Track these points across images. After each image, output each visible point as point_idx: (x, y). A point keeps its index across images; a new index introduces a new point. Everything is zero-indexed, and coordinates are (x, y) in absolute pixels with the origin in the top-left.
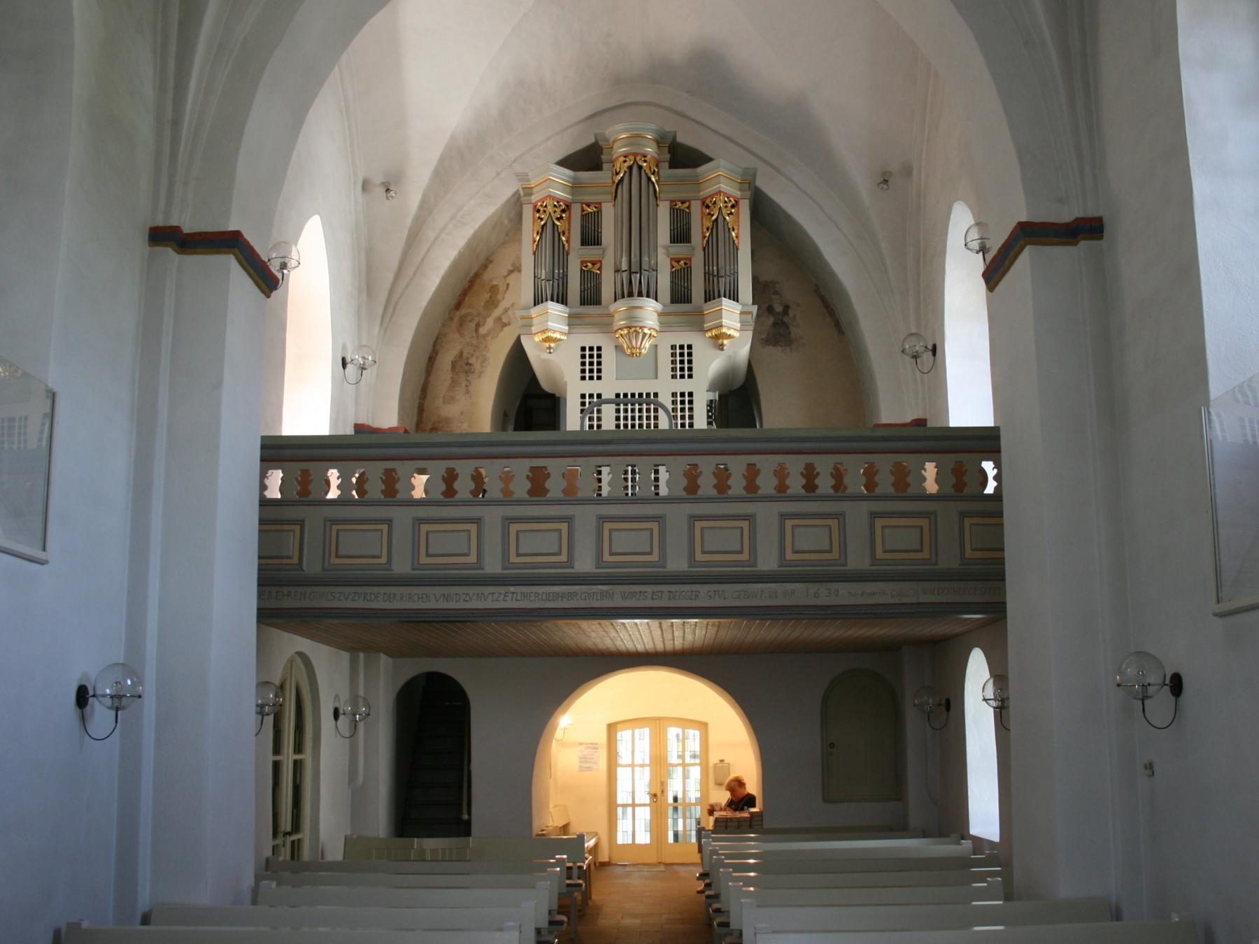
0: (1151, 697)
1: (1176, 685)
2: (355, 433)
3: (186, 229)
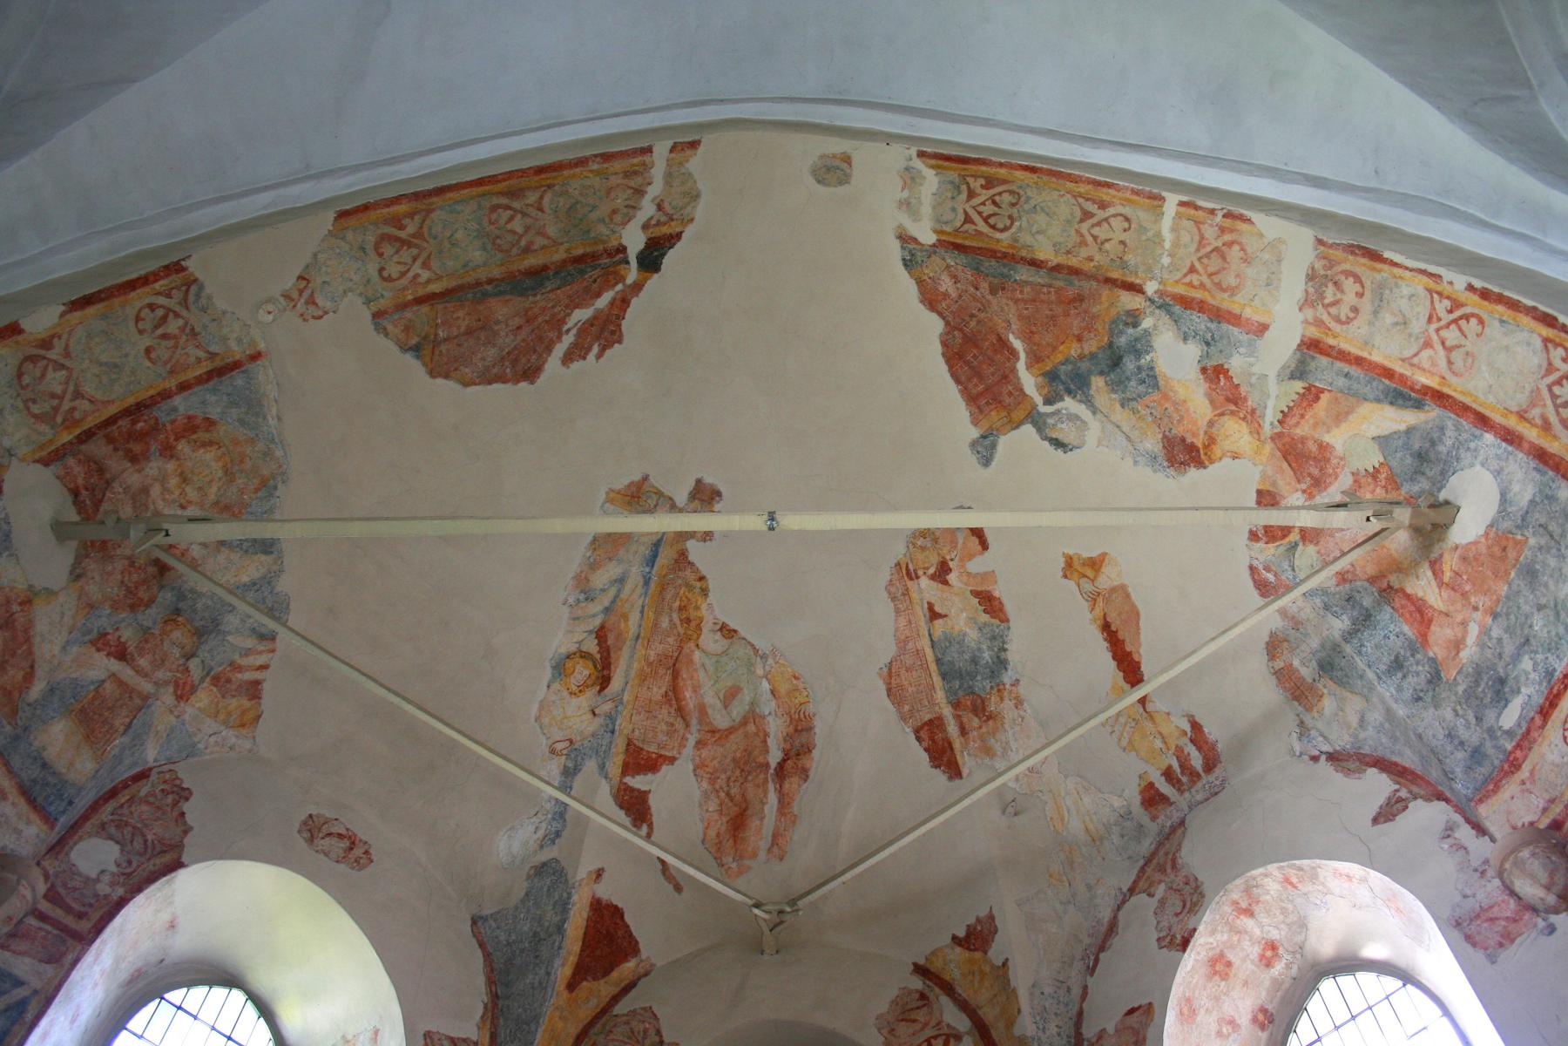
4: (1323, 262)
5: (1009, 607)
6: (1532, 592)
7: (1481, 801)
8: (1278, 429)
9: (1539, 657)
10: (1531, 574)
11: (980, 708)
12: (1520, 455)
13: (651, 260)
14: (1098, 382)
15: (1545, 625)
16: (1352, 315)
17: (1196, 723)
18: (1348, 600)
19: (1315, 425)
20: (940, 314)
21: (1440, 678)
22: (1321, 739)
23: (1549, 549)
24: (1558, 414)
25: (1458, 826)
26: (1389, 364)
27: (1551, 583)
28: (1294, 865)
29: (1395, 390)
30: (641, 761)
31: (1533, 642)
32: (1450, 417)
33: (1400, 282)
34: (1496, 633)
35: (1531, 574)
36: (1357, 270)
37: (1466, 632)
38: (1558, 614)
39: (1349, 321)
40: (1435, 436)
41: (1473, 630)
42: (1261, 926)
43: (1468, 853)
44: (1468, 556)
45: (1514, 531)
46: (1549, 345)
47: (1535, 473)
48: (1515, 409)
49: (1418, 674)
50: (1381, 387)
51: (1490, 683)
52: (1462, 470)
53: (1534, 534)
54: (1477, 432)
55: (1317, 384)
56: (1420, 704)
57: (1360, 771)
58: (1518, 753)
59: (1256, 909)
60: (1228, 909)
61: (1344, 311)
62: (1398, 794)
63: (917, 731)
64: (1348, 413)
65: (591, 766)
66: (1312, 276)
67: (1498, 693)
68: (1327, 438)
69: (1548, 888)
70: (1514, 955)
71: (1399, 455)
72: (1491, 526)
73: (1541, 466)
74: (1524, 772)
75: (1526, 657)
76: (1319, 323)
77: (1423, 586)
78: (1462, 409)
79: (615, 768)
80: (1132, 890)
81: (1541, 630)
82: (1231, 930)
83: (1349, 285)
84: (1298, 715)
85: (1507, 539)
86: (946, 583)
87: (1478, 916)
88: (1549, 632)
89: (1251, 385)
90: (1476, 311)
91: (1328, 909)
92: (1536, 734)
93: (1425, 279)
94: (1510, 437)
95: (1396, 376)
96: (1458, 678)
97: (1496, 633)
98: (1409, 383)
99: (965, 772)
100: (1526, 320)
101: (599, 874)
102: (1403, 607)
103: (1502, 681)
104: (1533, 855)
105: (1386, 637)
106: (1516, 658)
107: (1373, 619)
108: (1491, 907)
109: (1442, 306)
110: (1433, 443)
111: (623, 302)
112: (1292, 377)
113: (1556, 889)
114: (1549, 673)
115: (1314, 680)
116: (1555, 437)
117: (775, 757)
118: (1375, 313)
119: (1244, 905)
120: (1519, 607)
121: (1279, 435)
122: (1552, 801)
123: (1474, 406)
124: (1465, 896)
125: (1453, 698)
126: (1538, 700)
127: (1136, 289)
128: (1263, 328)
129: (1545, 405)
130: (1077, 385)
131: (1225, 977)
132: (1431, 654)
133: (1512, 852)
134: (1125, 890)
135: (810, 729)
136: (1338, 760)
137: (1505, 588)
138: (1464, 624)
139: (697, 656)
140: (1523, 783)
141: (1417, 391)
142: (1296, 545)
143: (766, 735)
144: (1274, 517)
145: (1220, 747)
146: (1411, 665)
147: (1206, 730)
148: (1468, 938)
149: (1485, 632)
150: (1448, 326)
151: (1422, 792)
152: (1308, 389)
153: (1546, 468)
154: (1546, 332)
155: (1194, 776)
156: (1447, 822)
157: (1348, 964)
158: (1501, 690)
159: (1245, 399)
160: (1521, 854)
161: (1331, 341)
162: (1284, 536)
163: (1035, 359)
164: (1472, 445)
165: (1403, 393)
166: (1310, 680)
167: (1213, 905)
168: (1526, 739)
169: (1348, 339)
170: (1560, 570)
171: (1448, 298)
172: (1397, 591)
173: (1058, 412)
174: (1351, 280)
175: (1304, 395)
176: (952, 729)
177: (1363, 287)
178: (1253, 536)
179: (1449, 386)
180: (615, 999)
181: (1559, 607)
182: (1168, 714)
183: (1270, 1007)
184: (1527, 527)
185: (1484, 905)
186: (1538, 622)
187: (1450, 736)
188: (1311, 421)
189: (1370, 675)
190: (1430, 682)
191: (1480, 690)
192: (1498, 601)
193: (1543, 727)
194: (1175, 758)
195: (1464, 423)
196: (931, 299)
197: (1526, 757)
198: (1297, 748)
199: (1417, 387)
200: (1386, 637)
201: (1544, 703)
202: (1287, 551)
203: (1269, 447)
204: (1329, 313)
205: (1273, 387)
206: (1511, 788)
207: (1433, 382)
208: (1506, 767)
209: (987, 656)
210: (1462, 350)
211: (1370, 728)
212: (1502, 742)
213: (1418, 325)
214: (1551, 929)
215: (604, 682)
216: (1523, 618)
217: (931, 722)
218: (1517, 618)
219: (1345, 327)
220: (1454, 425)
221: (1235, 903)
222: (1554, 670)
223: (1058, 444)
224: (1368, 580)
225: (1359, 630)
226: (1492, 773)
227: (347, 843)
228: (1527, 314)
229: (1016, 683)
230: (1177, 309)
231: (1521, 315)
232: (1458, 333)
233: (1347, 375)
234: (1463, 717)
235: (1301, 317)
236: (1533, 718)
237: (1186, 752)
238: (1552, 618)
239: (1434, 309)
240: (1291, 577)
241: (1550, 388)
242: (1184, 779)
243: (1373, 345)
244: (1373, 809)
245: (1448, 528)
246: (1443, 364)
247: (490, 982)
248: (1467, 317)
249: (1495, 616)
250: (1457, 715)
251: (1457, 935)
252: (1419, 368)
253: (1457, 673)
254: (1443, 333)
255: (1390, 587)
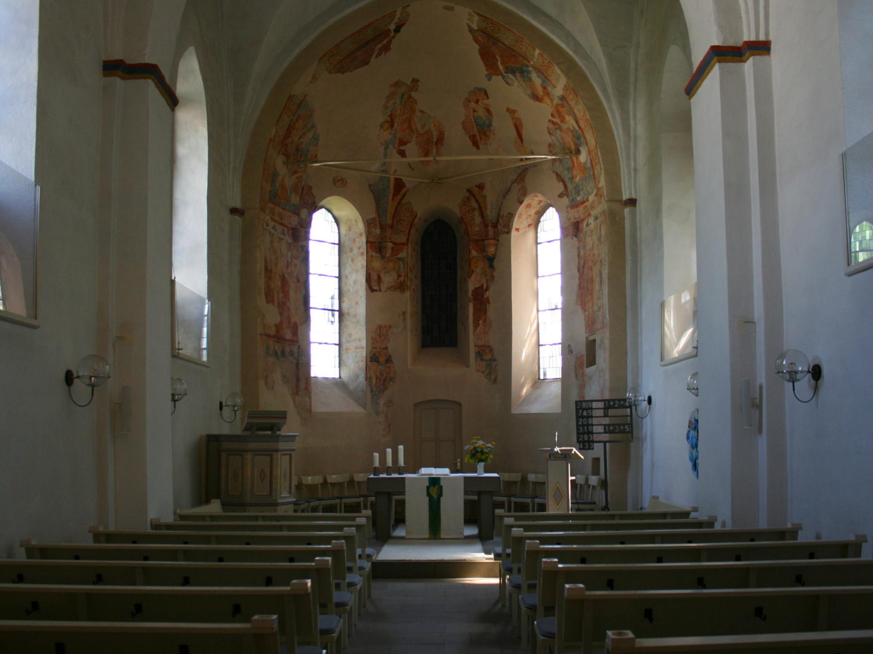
0: (799, 380)
1: (816, 372)
2: (861, 544)
3: (441, 498)
5: (493, 113)
11: (485, 134)
13: (397, 30)
14: (517, 74)
20: (479, 45)
30: (402, 143)
57: (560, 181)
63: (470, 137)
65: (391, 146)
79: (396, 146)
86: (478, 104)
99: (480, 148)
101: (395, 171)
111: (390, 41)
117: (435, 140)
127: (529, 62)
128: (555, 87)
130: (513, 73)
135: (444, 134)
139: (415, 117)
143: (433, 135)
163: (502, 63)
173: (507, 76)
176: (478, 138)
180: (402, 199)
196: (476, 41)
209: (487, 123)
215: (392, 126)
217: (473, 135)
223: (507, 83)
227: (341, 181)
229: (494, 130)
230: (538, 71)
247: (375, 201)
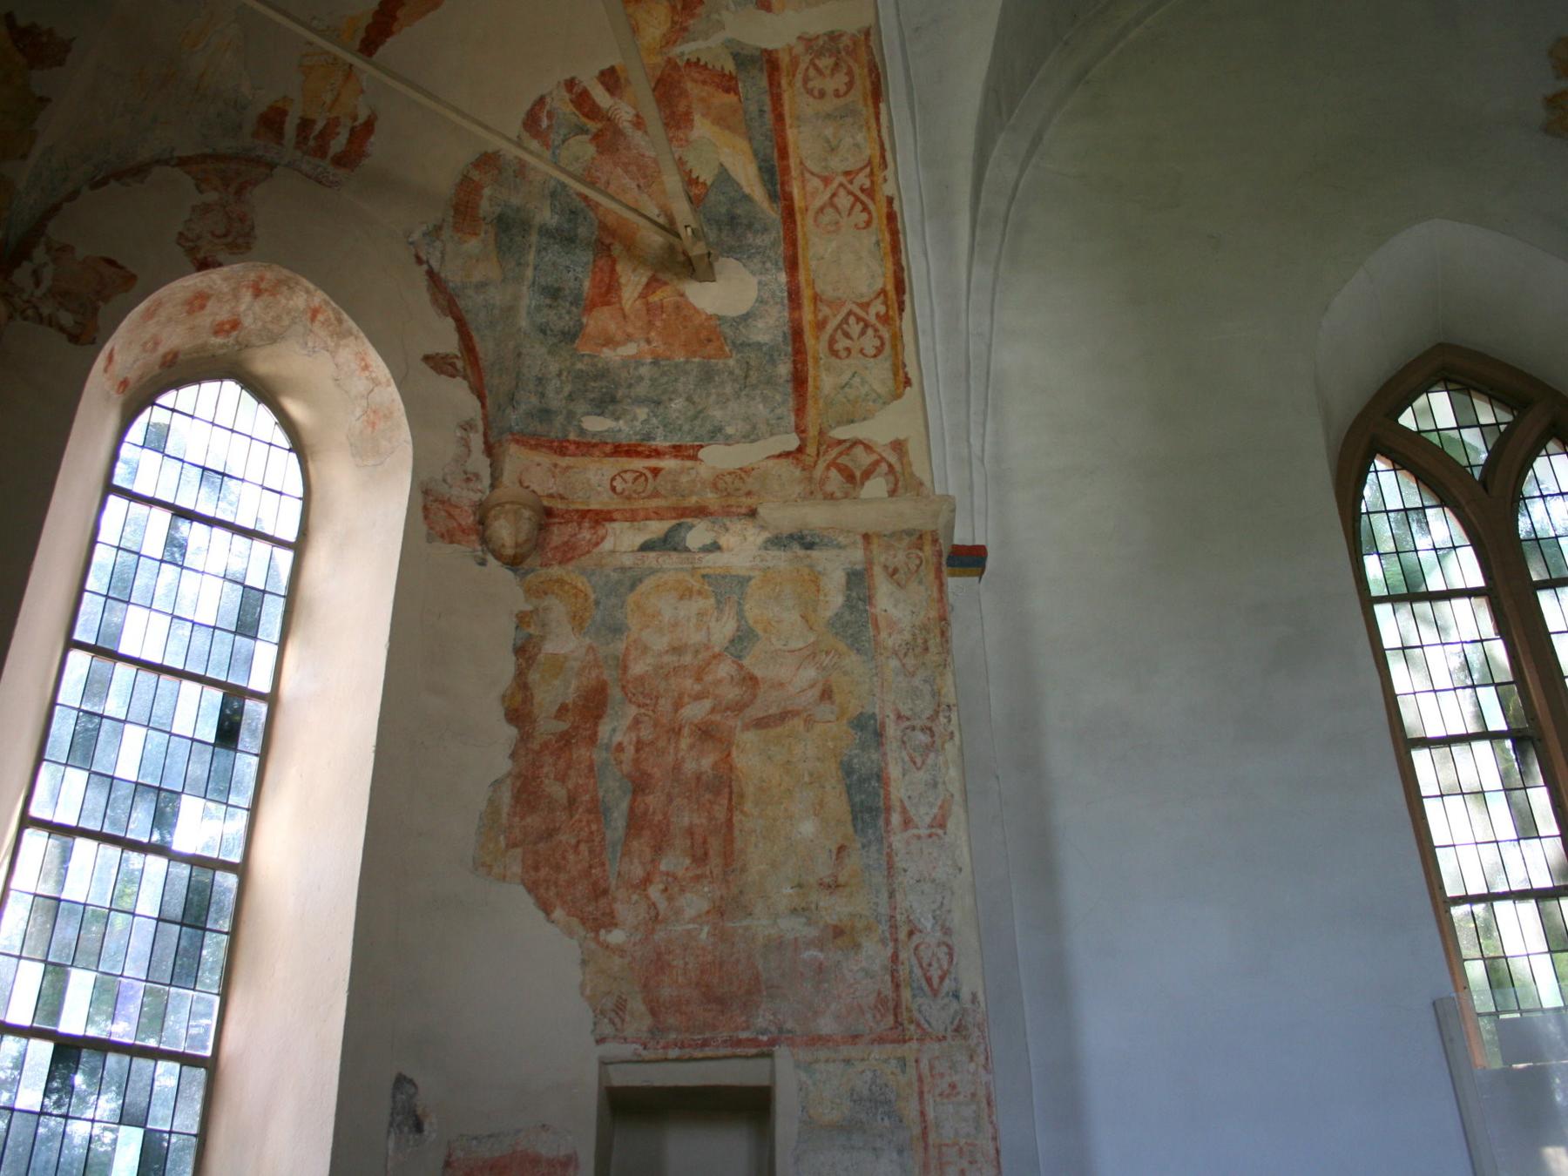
4: (850, 43)
6: (696, 385)
7: (517, 442)
8: (681, 63)
9: (654, 421)
10: (707, 376)
12: (786, 314)
15: (680, 412)
16: (816, 93)
17: (372, 125)
18: (572, 212)
19: (702, 100)
21: (573, 341)
22: (439, 255)
23: (735, 380)
24: (835, 330)
25: (477, 432)
26: (791, 149)
27: (713, 397)
28: (339, 313)
29: (773, 166)
31: (661, 409)
32: (778, 233)
33: (864, 129)
34: (643, 371)
35: (707, 376)
36: (858, 82)
37: (624, 343)
38: (695, 417)
39: (810, 92)
40: (757, 226)
41: (630, 349)
42: (249, 309)
43: (469, 455)
44: (682, 308)
45: (729, 341)
46: (882, 297)
47: (781, 334)
48: (818, 291)
49: (560, 318)
50: (768, 151)
51: (604, 390)
52: (745, 265)
53: (738, 361)
54: (781, 264)
55: (740, 85)
56: (541, 336)
58: (572, 447)
59: (265, 297)
60: (252, 276)
61: (816, 84)
62: (455, 360)
64: (729, 128)
66: (833, 37)
67: (602, 401)
68: (697, 117)
69: (517, 545)
70: (445, 550)
71: (722, 198)
72: (719, 318)
73: (789, 337)
74: (564, 462)
75: (646, 410)
76: (795, 62)
77: (632, 282)
78: (792, 241)
80: (183, 162)
81: (675, 411)
82: (234, 289)
83: (840, 80)
84: (444, 220)
85: (718, 339)
87: (443, 502)
88: (677, 418)
89: (708, 16)
90: (875, 214)
91: (310, 356)
92: (597, 453)
93: (878, 153)
94: (794, 296)
95: (785, 162)
96: (586, 358)
97: (643, 371)
98: (786, 178)
100: (890, 265)
102: (601, 270)
103: (613, 400)
104: (530, 519)
105: (568, 268)
106: (640, 401)
107: (573, 246)
108: (456, 507)
109: (862, 179)
110: (750, 226)
112: (736, 56)
113: (519, 550)
114: (649, 437)
115: (484, 219)
116: (817, 338)
118: (828, 116)
119: (263, 286)
120: (676, 380)
121: (676, 67)
122: (562, 497)
123: (800, 251)
124: (444, 481)
125: (568, 363)
126: (623, 440)
129: (835, 316)
131: (190, 312)
132: (584, 320)
133: (520, 504)
134: (176, 154)
136: (434, 282)
137: (682, 360)
138: (629, 338)
140: (555, 465)
141: (783, 191)
142: (586, 132)
144: (601, 97)
145: (366, 162)
146: (563, 308)
147: (372, 139)
148: (425, 508)
149: (637, 361)
150: (850, 193)
151: (472, 379)
152: (731, 77)
153: (790, 342)
154: (890, 288)
155: (321, 151)
156: (472, 419)
157: (264, 392)
158: (606, 403)
159: (693, 16)
160: (524, 511)
161: (784, 82)
162: (586, 115)
164: (768, 265)
165: (775, 171)
166: (481, 213)
167: (251, 264)
168: (587, 447)
169: (796, 101)
170: (728, 400)
171: (872, 182)
172: (610, 256)
174: (846, 79)
175: (724, 75)
177: (846, 93)
178: (570, 84)
179: (803, 219)
181: (702, 415)
182: (362, 91)
183: (181, 357)
184: (739, 352)
185: (454, 500)
186: (678, 404)
187: (540, 380)
188: (704, 94)
189: (529, 273)
190: (563, 333)
191: (593, 384)
192: (668, 359)
193: (607, 455)
194: (325, 122)
195: (782, 248)
197: (574, 455)
198: (416, 236)
199: (787, 188)
200: (568, 268)
201: (624, 446)
202: (576, 125)
203: (659, 60)
204: (807, 69)
205: (716, 40)
206: (544, 459)
207: (798, 202)
208: (556, 444)
210: (838, 217)
211: (482, 297)
212: (571, 429)
213: (837, 164)
214: (483, 563)
216: (671, 389)
218: (667, 383)
219: (802, 90)
220: (775, 239)
221: (262, 279)
222: (654, 439)
224: (600, 222)
225: (555, 238)
226: (542, 436)
228: (894, 264)
231: (891, 259)
232: (849, 206)
233: (762, 112)
234: (562, 382)
235: (793, 41)
236: (607, 443)
237: (338, 130)
238: (689, 414)
239: (857, 174)
240: (556, 143)
241: (850, 313)
242: (312, 143)
243: (799, 126)
244: (430, 351)
245: (691, 277)
246: (818, 203)
248: (865, 209)
249: (655, 363)
250: (559, 375)
251: (419, 498)
252: (803, 181)
253: (589, 355)
254: (842, 192)
255: (608, 247)
